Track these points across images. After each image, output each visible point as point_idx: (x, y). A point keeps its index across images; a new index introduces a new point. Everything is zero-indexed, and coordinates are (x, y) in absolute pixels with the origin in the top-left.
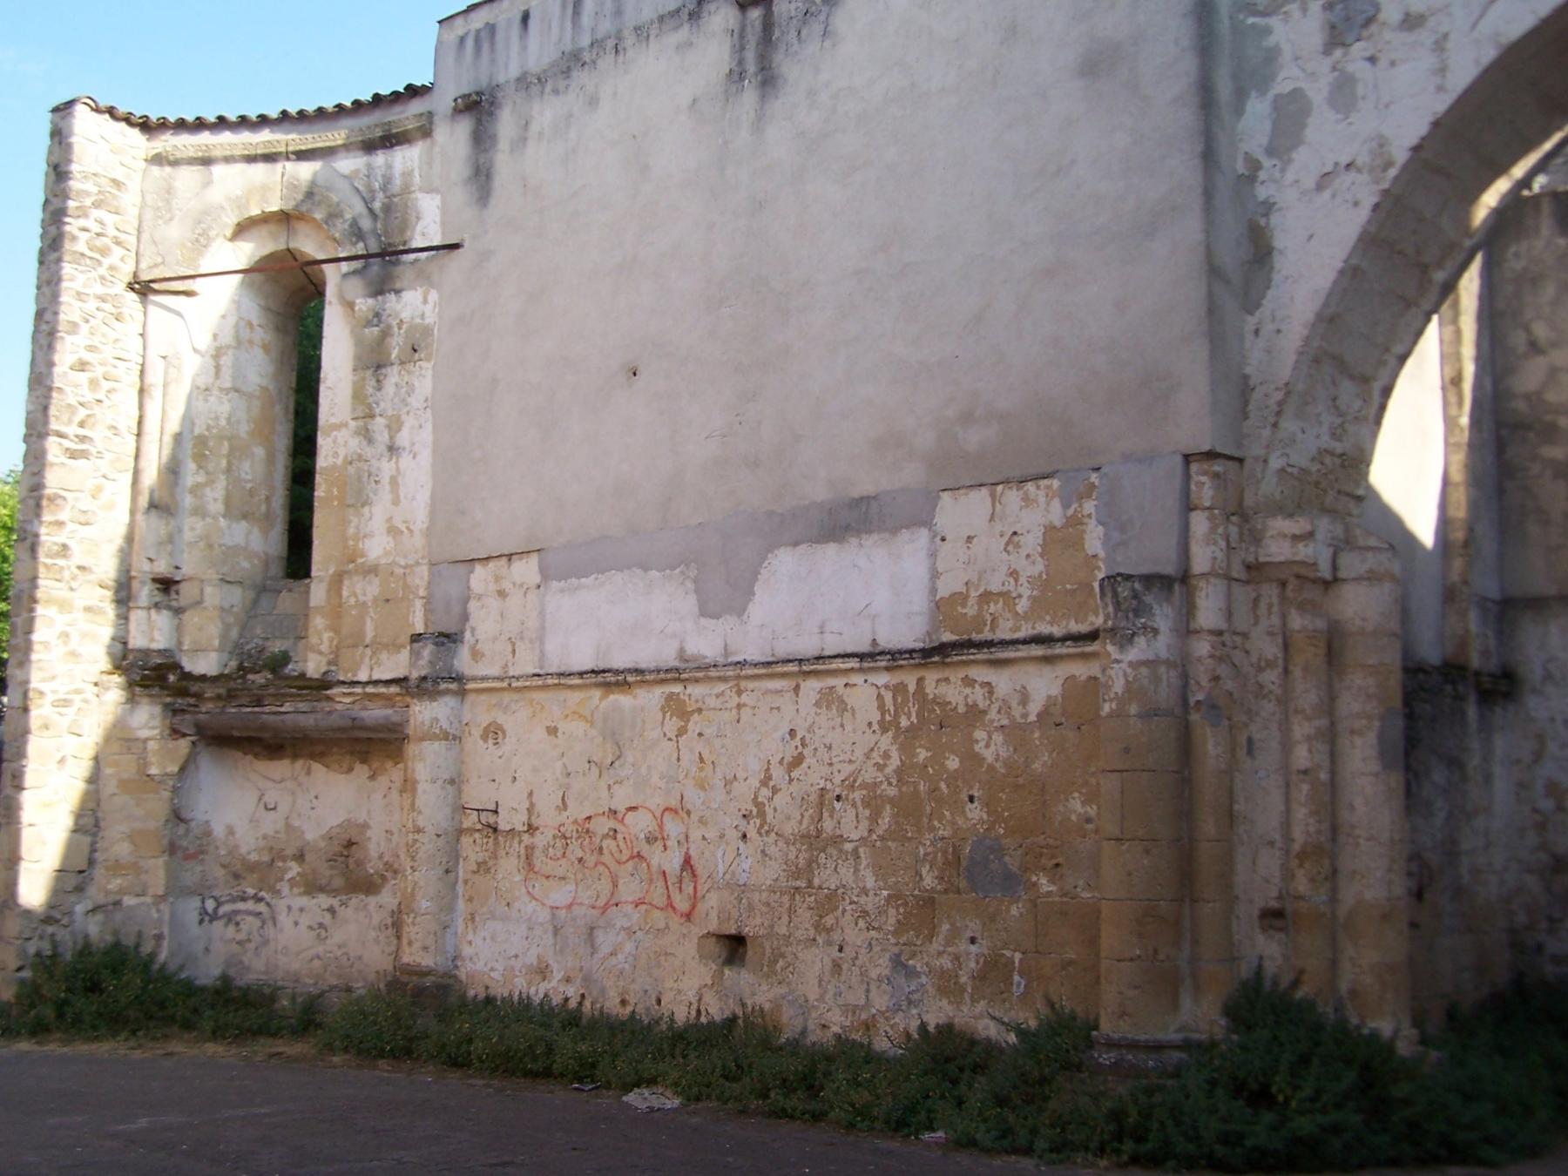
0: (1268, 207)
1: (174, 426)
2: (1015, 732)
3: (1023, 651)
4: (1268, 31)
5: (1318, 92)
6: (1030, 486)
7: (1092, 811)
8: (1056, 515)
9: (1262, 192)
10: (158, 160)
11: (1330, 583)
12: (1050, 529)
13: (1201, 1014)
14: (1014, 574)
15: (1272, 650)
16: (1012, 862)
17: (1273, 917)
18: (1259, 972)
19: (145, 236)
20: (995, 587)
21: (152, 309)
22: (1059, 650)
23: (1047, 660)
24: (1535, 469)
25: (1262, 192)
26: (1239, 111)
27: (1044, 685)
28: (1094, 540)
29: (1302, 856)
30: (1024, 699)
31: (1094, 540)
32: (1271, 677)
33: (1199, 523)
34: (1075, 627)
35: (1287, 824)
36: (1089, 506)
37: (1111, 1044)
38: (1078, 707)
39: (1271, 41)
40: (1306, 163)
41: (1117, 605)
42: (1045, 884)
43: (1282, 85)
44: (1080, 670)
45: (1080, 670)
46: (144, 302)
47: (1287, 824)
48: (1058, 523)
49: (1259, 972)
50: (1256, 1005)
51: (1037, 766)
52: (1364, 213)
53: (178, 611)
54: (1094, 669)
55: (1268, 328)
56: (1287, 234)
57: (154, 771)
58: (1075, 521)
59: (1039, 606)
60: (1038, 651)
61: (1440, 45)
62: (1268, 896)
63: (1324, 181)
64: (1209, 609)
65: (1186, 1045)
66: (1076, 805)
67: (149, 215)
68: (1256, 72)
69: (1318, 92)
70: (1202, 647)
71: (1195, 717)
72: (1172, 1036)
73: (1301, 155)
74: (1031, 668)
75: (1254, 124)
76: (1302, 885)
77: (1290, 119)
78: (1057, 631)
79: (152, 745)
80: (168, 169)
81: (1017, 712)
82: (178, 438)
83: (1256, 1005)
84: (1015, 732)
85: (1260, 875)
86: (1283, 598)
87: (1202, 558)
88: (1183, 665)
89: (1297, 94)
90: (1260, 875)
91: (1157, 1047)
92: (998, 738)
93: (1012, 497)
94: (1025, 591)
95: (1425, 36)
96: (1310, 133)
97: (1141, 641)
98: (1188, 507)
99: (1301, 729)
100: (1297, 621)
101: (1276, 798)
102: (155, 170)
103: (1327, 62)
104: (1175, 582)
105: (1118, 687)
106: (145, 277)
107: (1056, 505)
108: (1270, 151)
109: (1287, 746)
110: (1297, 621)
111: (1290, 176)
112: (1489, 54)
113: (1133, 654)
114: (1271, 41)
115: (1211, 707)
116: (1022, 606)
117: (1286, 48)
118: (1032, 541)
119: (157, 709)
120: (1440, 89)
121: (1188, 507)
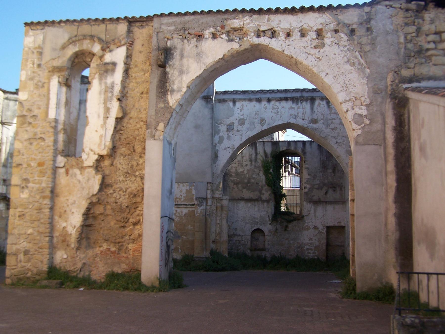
0: (218, 150)
1: (8, 151)
2: (180, 217)
3: (183, 206)
4: (219, 127)
5: (225, 137)
6: (184, 184)
7: (192, 228)
8: (188, 188)
9: (217, 148)
10: (7, 99)
11: (222, 200)
12: (187, 190)
13: (207, 254)
14: (181, 196)
15: (215, 208)
16: (179, 234)
17: (213, 242)
18: (212, 248)
19: (4, 114)
20: (178, 197)
21: (4, 128)
22: (188, 206)
23: (186, 207)
24: (229, 180)
25: (217, 148)
26: (214, 137)
27: (185, 211)
28: (194, 192)
29: (218, 234)
30: (182, 213)
31: (194, 192)
32: (214, 211)
33: (209, 192)
34: (190, 203)
35: (216, 230)
36: (193, 188)
37: (197, 258)
38: (191, 215)
39: (219, 128)
40: (223, 145)
41: (199, 201)
42: (184, 237)
43: (221, 134)
44: (191, 209)
45: (191, 209)
46: (2, 126)
47: (216, 230)
48: (188, 189)
49: (212, 248)
50: (213, 253)
51: (184, 222)
52: (231, 154)
53: (7, 186)
54: (193, 209)
55: (217, 166)
56: (220, 154)
57: (4, 216)
58: (191, 189)
59: (185, 200)
60: (185, 206)
61: (241, 135)
62: (213, 239)
63: (225, 149)
64: (209, 202)
65: (206, 258)
66: (190, 227)
67: (4, 109)
68: (218, 132)
69: (225, 137)
70: (208, 207)
71: (207, 216)
72: (204, 256)
73: (222, 144)
74: (183, 209)
75: (216, 139)
76: (218, 238)
77: (221, 139)
78: (187, 204)
79: (3, 211)
80: (8, 101)
81: (181, 214)
82: (9, 153)
83: (213, 253)
84: (180, 217)
85: (212, 237)
86: (216, 202)
87: (209, 196)
88: (206, 209)
89: (222, 136)
90: (212, 237)
91: (203, 258)
92: (178, 218)
93: (181, 185)
94: (183, 198)
95: (240, 133)
96: (224, 142)
97: (202, 206)
98: (207, 189)
99: (218, 218)
100: (218, 204)
101: (215, 226)
102: (6, 101)
103: (227, 133)
104: (206, 199)
105: (199, 212)
106: (4, 121)
107: (188, 187)
108: (218, 143)
109: (216, 220)
110: (218, 204)
111: (221, 147)
112: (247, 138)
113: (201, 208)
114: (219, 128)
115: (209, 215)
116: (182, 200)
117: (221, 131)
118: (184, 191)
119: (4, 204)
120: (241, 140)
121: (207, 189)
